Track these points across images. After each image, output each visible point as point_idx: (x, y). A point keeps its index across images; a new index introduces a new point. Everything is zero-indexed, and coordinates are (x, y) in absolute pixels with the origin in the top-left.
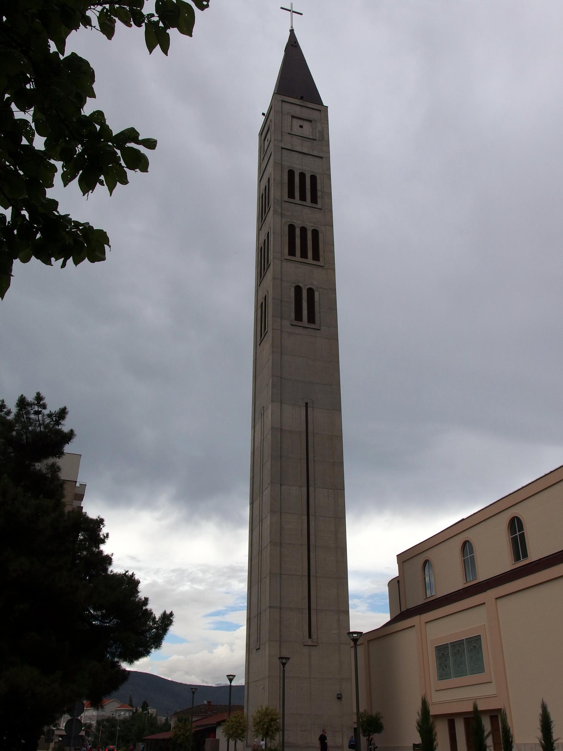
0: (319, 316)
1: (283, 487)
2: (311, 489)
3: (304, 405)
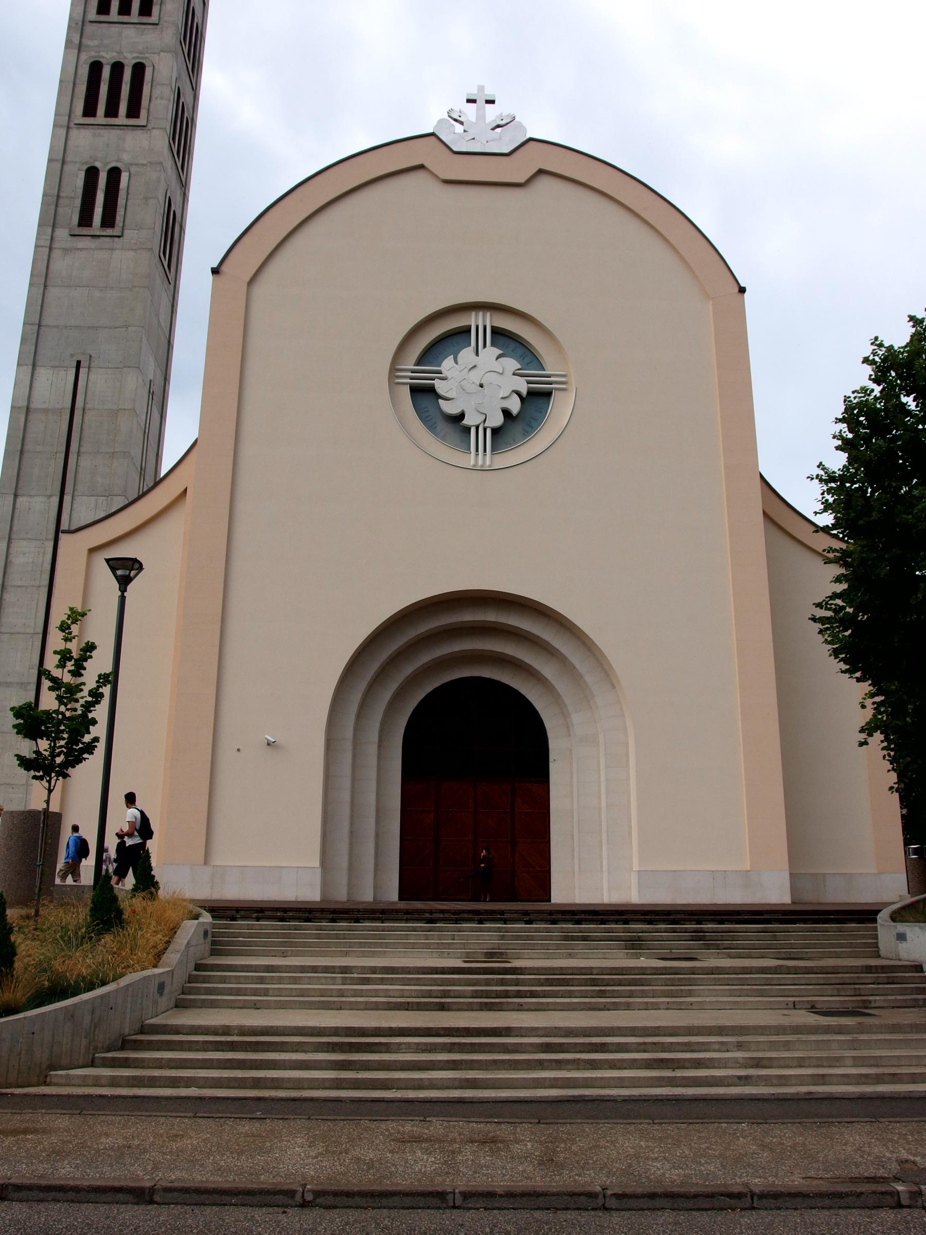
0: (123, 213)
1: (20, 500)
2: (67, 499)
3: (75, 364)
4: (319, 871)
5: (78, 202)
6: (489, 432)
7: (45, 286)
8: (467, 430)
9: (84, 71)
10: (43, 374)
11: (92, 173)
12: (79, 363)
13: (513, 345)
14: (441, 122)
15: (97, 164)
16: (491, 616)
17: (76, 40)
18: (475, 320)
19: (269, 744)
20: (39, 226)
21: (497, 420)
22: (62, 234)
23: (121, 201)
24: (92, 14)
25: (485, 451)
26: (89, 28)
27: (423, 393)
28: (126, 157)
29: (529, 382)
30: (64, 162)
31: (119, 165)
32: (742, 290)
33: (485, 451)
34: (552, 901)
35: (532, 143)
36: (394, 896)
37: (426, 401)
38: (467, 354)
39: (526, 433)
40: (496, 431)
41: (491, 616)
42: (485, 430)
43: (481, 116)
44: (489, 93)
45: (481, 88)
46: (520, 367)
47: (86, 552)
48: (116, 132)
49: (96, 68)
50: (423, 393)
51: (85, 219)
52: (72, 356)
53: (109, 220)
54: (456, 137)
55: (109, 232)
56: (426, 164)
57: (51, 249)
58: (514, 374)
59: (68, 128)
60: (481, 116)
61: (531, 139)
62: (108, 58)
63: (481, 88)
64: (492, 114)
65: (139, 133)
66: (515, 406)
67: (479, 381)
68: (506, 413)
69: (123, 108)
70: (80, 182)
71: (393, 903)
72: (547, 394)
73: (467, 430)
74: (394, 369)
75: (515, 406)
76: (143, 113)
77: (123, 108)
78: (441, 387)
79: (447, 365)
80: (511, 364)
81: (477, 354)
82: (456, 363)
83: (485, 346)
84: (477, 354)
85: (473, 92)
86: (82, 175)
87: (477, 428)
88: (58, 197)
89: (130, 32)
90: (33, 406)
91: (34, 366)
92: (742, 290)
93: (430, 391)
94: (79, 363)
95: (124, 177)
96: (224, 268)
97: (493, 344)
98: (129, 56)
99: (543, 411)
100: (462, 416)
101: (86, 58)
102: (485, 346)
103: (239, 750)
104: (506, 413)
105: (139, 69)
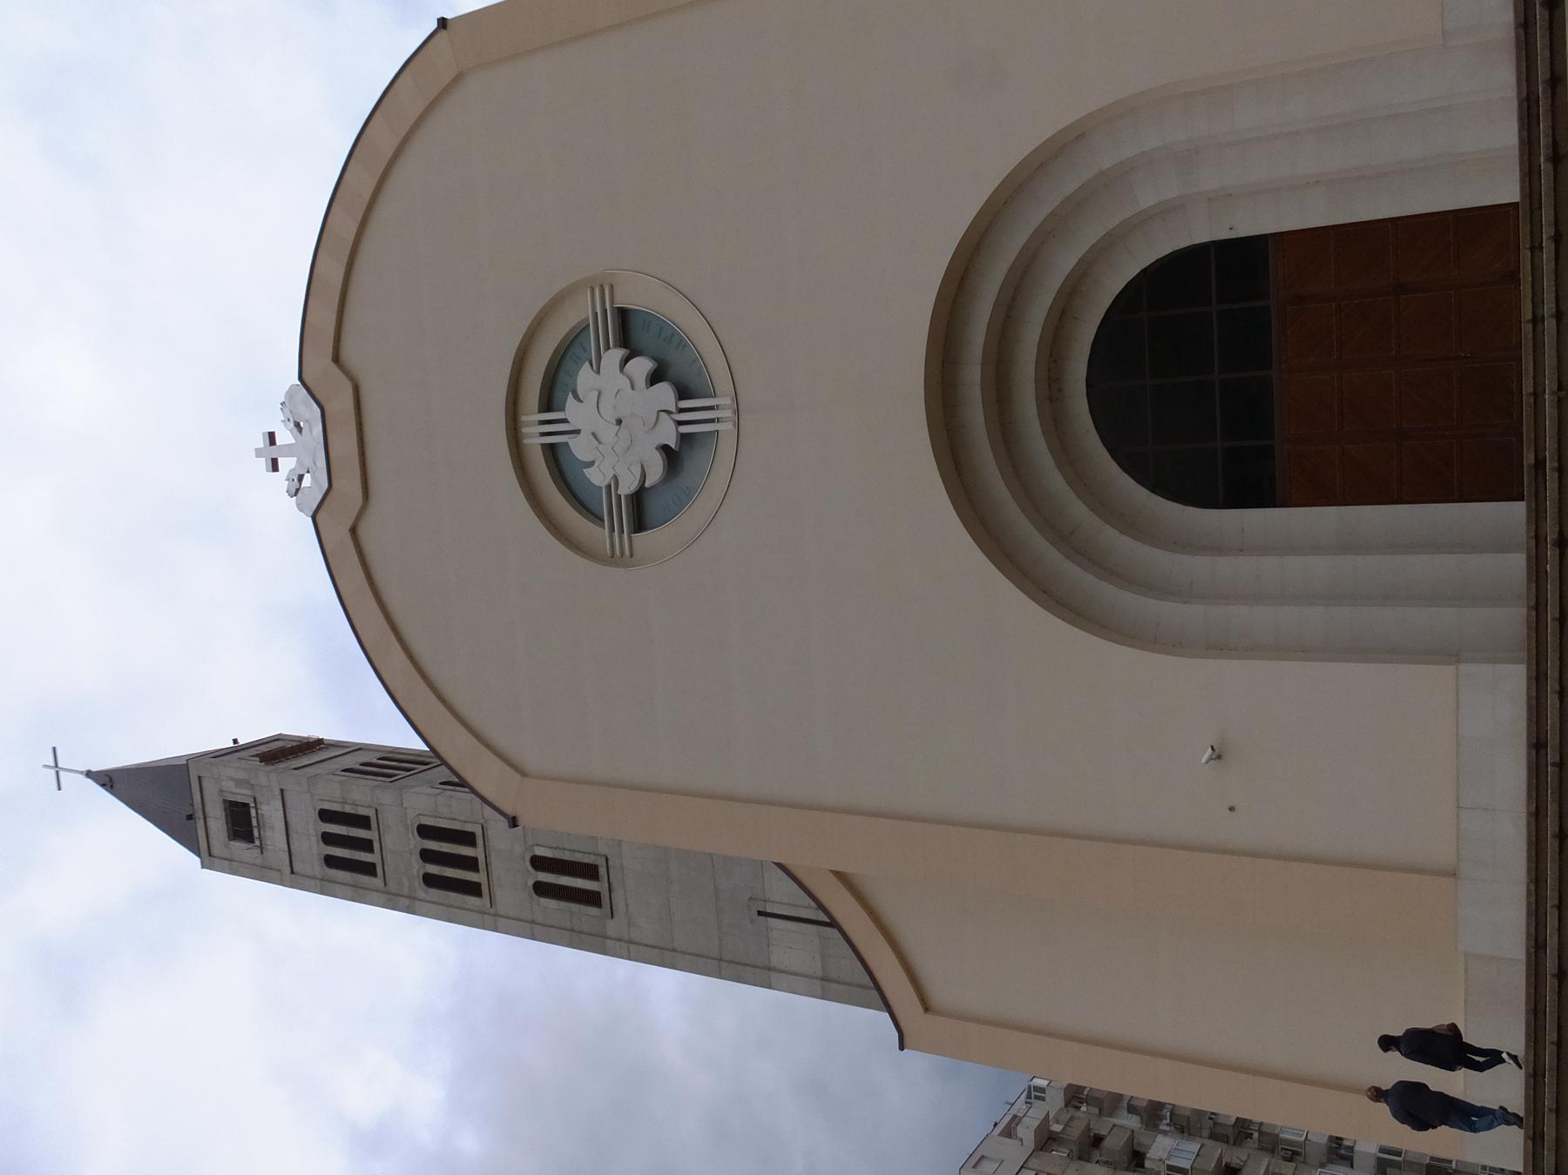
4: (1464, 668)
5: (574, 907)
6: (685, 404)
7: (674, 950)
8: (684, 438)
9: (436, 894)
10: (778, 958)
11: (541, 889)
12: (760, 913)
13: (562, 376)
14: (300, 507)
15: (531, 883)
16: (973, 374)
17: (406, 902)
18: (534, 438)
19: (1219, 757)
20: (605, 953)
21: (665, 392)
22: (612, 927)
23: (567, 856)
24: (377, 882)
25: (711, 408)
26: (392, 887)
27: (640, 511)
28: (518, 849)
29: (608, 348)
30: (533, 922)
31: (528, 858)
32: (443, 23)
33: (711, 408)
34: (1517, 199)
35: (305, 376)
36: (1514, 513)
37: (653, 507)
38: (580, 448)
39: (682, 345)
40: (683, 393)
41: (973, 374)
42: (682, 411)
43: (289, 450)
44: (261, 442)
45: (259, 453)
46: (587, 364)
47: (929, 1016)
48: (494, 860)
49: (430, 881)
50: (640, 511)
51: (592, 899)
52: (752, 922)
53: (590, 871)
54: (314, 484)
55: (602, 871)
56: (349, 525)
57: (631, 942)
58: (598, 372)
59: (496, 915)
60: (289, 450)
61: (300, 378)
62: (418, 867)
63: (259, 453)
64: (285, 437)
65: (490, 833)
66: (641, 366)
67: (615, 425)
68: (654, 378)
69: (466, 851)
70: (552, 904)
71: (1528, 507)
72: (623, 315)
73: (684, 438)
74: (613, 559)
75: (641, 366)
76: (468, 828)
77: (466, 851)
78: (628, 486)
79: (597, 477)
80: (585, 377)
81: (577, 432)
82: (591, 464)
83: (565, 421)
84: (577, 432)
85: (263, 463)
86: (544, 901)
87: (680, 423)
88: (572, 930)
89: (389, 841)
90: (819, 973)
91: (769, 969)
92: (443, 23)
93: (638, 499)
94: (760, 913)
95: (540, 852)
96: (509, 811)
97: (563, 410)
98: (413, 842)
99: (649, 319)
100: (665, 448)
101: (422, 892)
102: (565, 421)
103: (1231, 809)
104: (654, 378)
105: (425, 831)
